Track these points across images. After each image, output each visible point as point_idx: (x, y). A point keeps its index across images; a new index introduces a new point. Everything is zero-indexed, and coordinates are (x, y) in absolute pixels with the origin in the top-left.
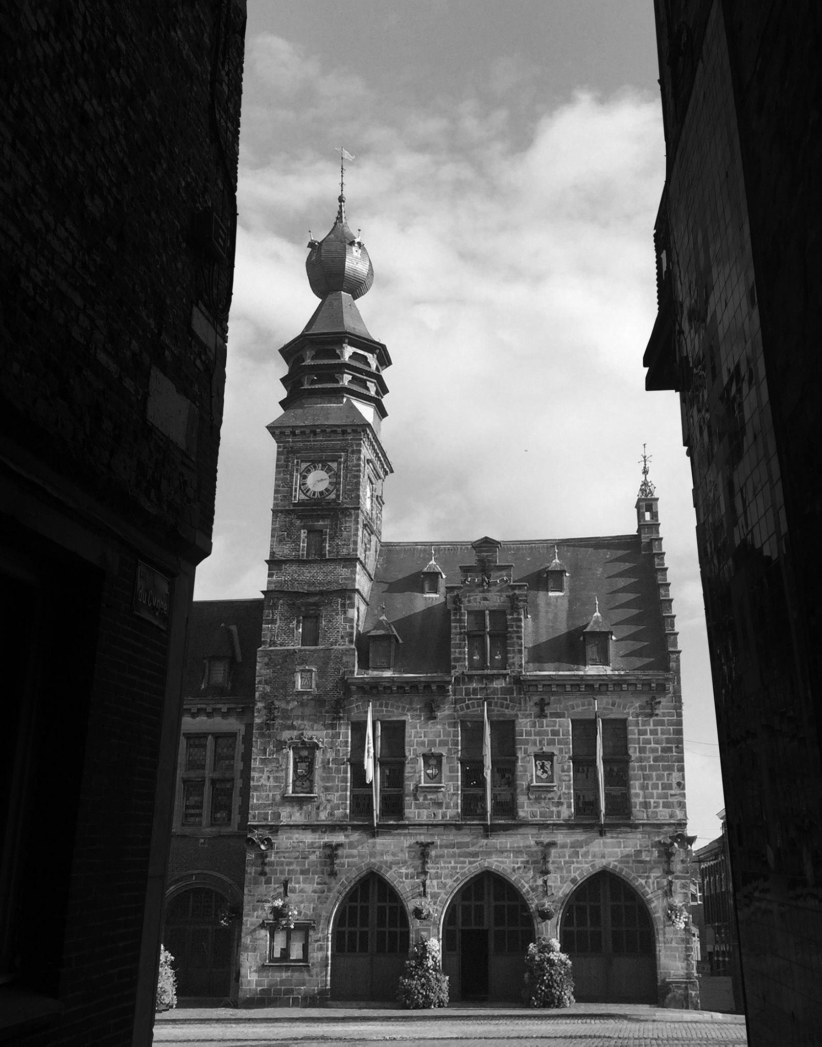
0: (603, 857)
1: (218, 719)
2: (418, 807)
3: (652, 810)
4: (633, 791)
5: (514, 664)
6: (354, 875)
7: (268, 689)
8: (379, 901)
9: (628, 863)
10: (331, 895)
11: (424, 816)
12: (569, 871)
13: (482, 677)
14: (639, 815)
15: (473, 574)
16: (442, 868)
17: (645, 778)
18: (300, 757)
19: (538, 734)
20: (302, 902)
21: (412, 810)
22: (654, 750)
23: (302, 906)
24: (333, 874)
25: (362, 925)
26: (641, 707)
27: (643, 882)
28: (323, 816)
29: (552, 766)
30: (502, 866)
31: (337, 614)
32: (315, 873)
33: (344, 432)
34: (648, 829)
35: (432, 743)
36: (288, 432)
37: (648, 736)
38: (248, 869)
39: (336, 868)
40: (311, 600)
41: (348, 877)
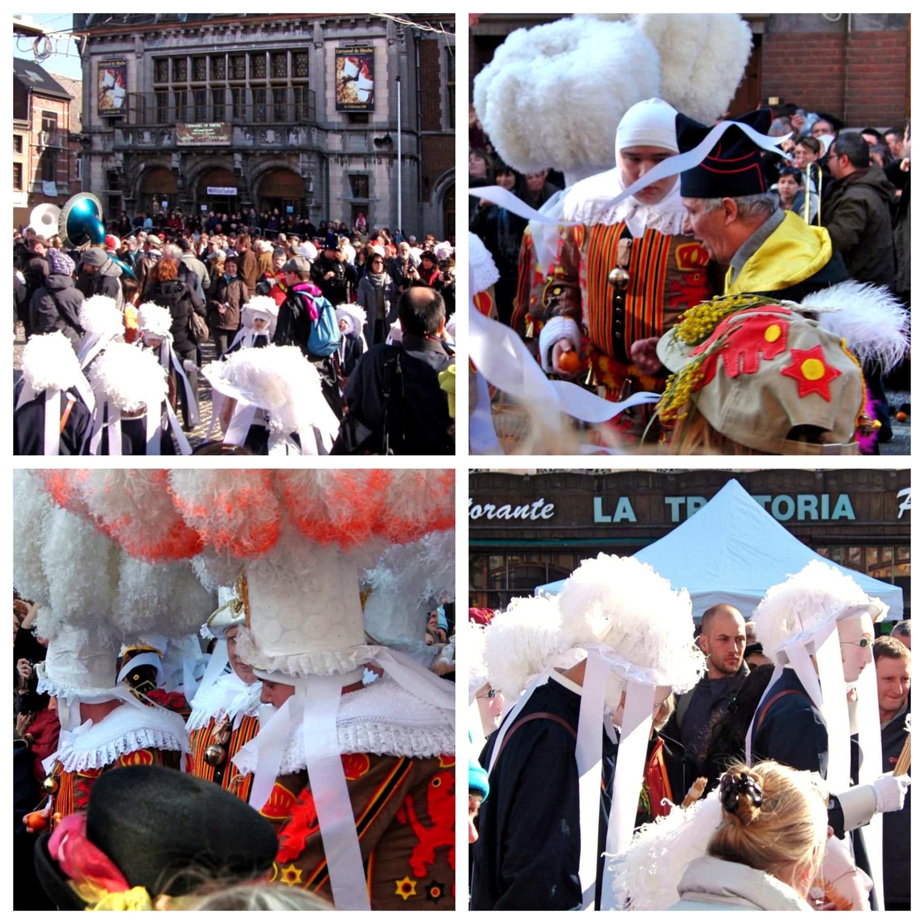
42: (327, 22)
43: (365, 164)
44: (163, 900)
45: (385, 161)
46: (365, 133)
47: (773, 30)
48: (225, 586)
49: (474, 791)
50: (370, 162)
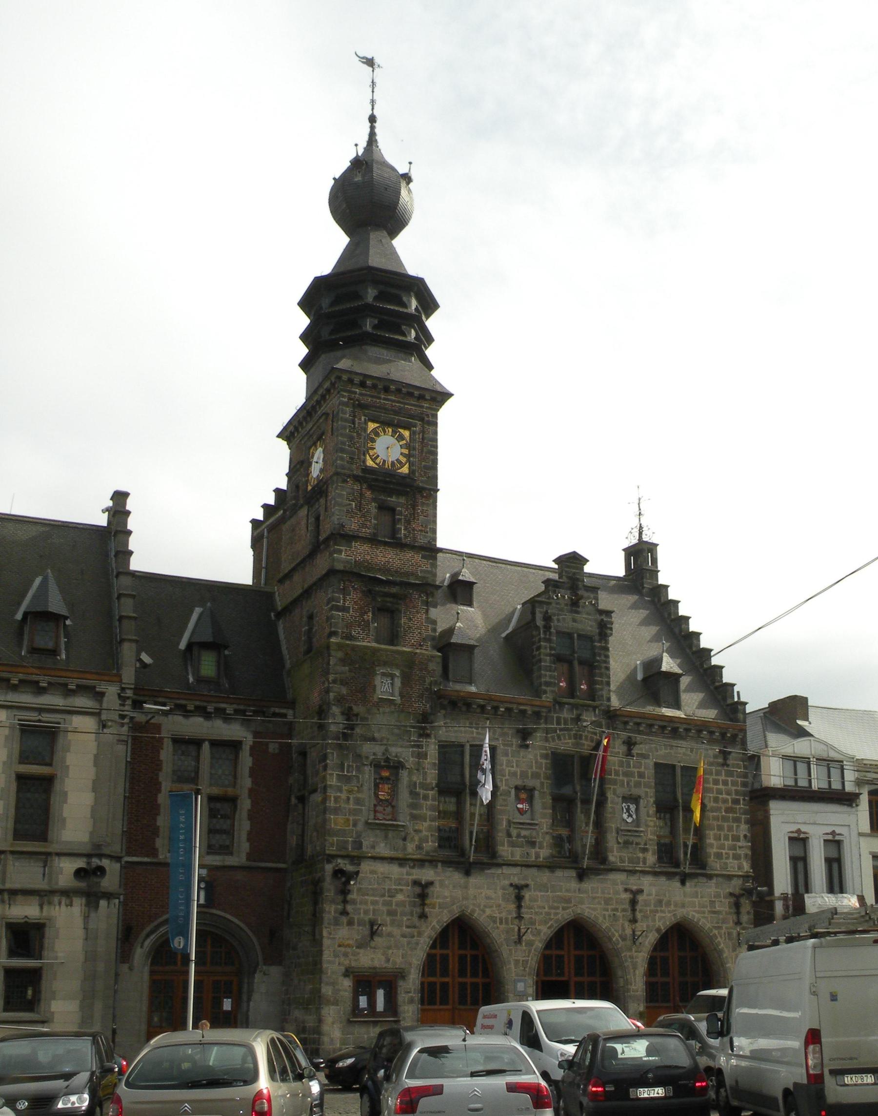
0: (683, 906)
1: (218, 723)
2: (513, 845)
3: (724, 861)
4: (708, 841)
5: (602, 696)
6: (446, 918)
7: (344, 691)
8: (459, 948)
9: (704, 913)
10: (422, 940)
11: (517, 854)
12: (654, 920)
13: (574, 706)
14: (715, 865)
15: (562, 591)
16: (536, 913)
17: (720, 828)
18: (381, 778)
19: (626, 774)
20: (389, 948)
21: (506, 848)
22: (725, 801)
23: (390, 951)
24: (423, 916)
25: (442, 975)
26: (715, 757)
27: (716, 932)
28: (411, 847)
29: (637, 810)
30: (594, 913)
31: (418, 612)
32: (403, 914)
33: (421, 397)
34: (720, 879)
35: (524, 775)
36: (357, 380)
37: (720, 786)
38: (327, 907)
39: (427, 910)
40: (394, 590)
41: (439, 918)
42: (21, 681)
43: (41, 906)
44: (607, 562)
45: (79, 903)
46: (45, 857)
47: (631, 896)
48: (320, 989)
49: (484, 772)
50: (50, 903)
